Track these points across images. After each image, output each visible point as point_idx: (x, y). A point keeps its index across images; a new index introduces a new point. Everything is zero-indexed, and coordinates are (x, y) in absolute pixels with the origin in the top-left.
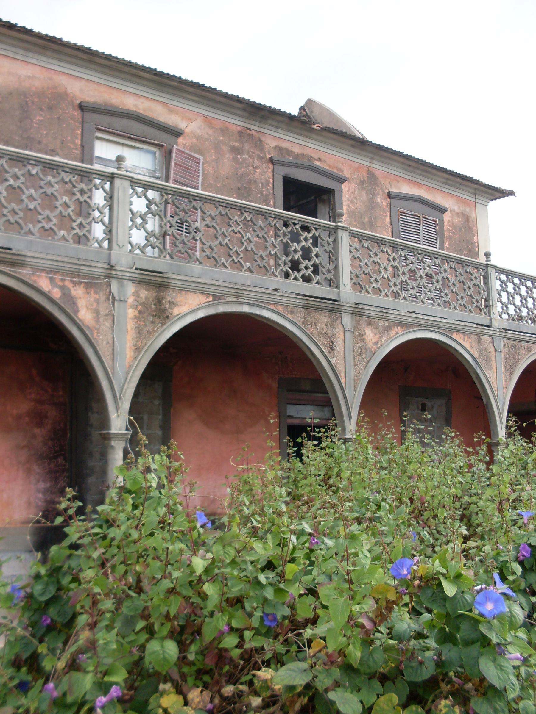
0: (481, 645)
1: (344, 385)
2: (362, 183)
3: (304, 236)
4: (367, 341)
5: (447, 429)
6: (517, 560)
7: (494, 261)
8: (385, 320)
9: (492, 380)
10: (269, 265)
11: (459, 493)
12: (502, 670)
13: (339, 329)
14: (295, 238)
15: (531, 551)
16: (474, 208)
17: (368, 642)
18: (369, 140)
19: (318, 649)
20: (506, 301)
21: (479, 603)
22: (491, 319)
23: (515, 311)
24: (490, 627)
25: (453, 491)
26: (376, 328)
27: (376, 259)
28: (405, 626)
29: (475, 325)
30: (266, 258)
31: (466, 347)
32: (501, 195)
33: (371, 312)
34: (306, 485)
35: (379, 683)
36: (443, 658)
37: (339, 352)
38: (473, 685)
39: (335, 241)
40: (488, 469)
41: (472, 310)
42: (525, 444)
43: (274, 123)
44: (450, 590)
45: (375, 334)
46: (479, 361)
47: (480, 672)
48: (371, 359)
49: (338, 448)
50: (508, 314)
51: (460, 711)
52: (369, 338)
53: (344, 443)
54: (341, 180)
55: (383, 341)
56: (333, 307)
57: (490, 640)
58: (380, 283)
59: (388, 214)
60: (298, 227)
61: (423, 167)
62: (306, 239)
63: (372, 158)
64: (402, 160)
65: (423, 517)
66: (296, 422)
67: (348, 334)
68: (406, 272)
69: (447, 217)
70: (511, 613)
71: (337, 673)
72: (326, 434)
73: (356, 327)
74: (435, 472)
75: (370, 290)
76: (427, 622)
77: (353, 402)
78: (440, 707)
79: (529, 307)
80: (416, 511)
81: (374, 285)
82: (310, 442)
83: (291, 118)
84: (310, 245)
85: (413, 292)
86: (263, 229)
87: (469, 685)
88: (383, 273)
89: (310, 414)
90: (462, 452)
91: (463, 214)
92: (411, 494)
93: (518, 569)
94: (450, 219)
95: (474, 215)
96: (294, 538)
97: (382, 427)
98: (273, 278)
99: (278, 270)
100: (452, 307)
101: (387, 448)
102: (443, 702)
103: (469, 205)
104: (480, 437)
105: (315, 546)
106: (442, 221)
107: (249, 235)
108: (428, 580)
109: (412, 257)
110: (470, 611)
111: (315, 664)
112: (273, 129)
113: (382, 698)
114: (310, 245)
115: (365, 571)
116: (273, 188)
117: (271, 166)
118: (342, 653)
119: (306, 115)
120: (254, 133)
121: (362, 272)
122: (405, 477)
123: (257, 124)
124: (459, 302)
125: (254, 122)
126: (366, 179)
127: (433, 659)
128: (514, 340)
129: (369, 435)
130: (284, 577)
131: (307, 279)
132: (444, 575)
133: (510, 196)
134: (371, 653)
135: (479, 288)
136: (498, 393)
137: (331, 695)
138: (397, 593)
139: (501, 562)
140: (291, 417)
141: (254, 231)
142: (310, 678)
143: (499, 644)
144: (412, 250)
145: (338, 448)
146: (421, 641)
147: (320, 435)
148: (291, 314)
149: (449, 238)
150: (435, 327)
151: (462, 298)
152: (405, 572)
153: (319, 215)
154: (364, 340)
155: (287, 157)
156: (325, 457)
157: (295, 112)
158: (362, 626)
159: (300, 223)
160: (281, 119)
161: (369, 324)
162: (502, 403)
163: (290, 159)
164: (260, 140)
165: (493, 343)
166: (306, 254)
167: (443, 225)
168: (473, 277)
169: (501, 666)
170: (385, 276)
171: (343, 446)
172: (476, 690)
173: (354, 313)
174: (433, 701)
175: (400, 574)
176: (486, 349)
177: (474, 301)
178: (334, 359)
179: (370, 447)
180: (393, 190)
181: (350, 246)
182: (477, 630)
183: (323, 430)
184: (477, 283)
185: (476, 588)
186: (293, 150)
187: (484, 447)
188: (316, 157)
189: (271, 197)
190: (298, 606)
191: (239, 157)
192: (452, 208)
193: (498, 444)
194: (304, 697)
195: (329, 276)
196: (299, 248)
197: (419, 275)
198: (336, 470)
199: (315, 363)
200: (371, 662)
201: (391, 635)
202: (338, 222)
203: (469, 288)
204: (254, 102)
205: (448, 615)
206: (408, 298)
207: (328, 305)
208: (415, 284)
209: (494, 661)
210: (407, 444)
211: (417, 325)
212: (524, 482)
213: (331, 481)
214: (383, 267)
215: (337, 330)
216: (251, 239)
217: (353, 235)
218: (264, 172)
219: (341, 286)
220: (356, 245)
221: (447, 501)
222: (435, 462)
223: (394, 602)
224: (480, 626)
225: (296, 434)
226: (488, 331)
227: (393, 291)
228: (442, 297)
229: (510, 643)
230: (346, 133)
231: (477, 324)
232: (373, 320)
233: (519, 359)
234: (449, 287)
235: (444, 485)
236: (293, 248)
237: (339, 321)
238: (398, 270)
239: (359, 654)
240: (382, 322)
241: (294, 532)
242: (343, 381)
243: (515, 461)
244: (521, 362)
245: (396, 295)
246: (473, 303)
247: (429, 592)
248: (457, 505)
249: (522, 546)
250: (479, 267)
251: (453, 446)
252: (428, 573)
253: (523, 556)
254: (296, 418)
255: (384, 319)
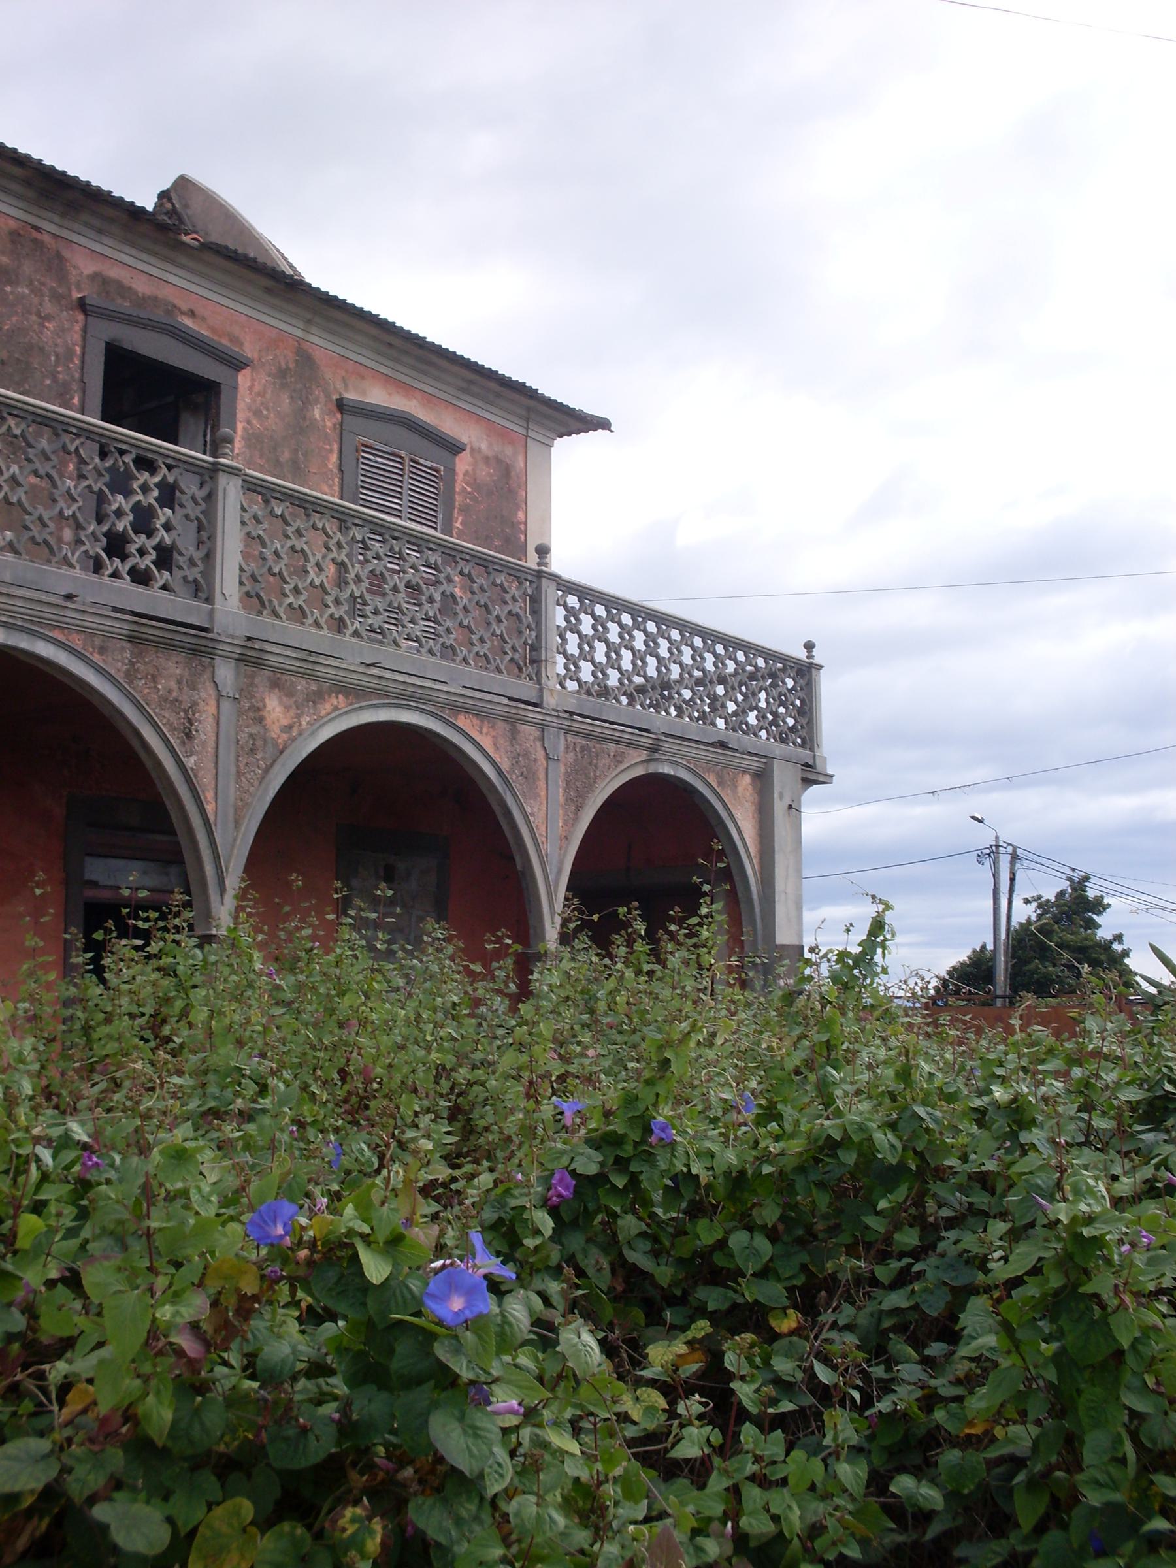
0: (436, 1387)
1: (212, 818)
2: (282, 373)
3: (141, 481)
4: (268, 721)
5: (430, 924)
6: (545, 1203)
7: (558, 564)
8: (310, 678)
9: (538, 821)
10: (60, 540)
11: (450, 1060)
12: (476, 1436)
13: (206, 693)
14: (121, 484)
15: (575, 1186)
16: (522, 450)
17: (192, 1386)
18: (308, 280)
19: (80, 1407)
20: (576, 652)
21: (432, 1296)
22: (541, 690)
23: (594, 674)
24: (458, 1349)
25: (434, 1056)
26: (290, 694)
27: (300, 544)
28: (286, 1350)
29: (506, 701)
30: (51, 525)
31: (483, 746)
32: (580, 426)
33: (281, 660)
34: (110, 1037)
35: (213, 1478)
36: (355, 1417)
37: (204, 744)
38: (415, 1472)
39: (210, 497)
40: (514, 1010)
41: (503, 668)
42: (595, 959)
43: (97, 223)
44: (375, 1269)
45: (287, 708)
46: (512, 778)
47: (430, 1445)
48: (275, 761)
49: (187, 956)
50: (579, 681)
51: (384, 1528)
52: (274, 716)
53: (200, 946)
54: (237, 364)
55: (304, 723)
56: (198, 644)
57: (458, 1376)
58: (303, 597)
59: (336, 447)
60: (128, 459)
61: (419, 352)
62: (145, 488)
63: (309, 322)
64: (374, 331)
65: (368, 1112)
66: (105, 895)
67: (226, 705)
68: (363, 575)
69: (463, 464)
70: (504, 1316)
71: (116, 1458)
72: (161, 924)
73: (246, 691)
74: (396, 1014)
75: (280, 611)
76: (331, 1339)
77: (230, 856)
78: (342, 1522)
79: (624, 668)
80: (354, 1099)
81: (291, 599)
82: (124, 942)
83: (134, 212)
84: (153, 501)
85: (375, 621)
86: (48, 459)
87: (409, 1472)
88: (312, 574)
89: (131, 879)
90: (459, 973)
91: (498, 460)
92: (343, 1061)
93: (546, 1223)
94: (470, 469)
95: (522, 464)
96: (46, 1155)
97: (288, 914)
98: (65, 570)
99: (77, 554)
100: (458, 659)
101: (299, 959)
102: (349, 1512)
103: (512, 442)
104: (499, 940)
105: (94, 1172)
106: (451, 471)
107: (15, 469)
108: (331, 1249)
109: (378, 545)
110: (418, 1314)
111: (69, 1441)
112: (92, 234)
113: (218, 1511)
114: (153, 501)
115: (187, 1230)
116: (82, 369)
117: (81, 317)
118: (129, 1415)
119: (174, 212)
120: (46, 238)
121: (265, 569)
122: (332, 1025)
123: (57, 218)
124: (476, 649)
125: (49, 215)
126: (292, 365)
127: (333, 1420)
128: (588, 736)
129: (257, 930)
130: (13, 1244)
131: (141, 578)
132: (364, 1237)
133: (600, 431)
134: (197, 1412)
135: (520, 621)
136: (549, 848)
137: (100, 1512)
138: (262, 1277)
139: (513, 1209)
140: (94, 884)
141: (29, 460)
142: (54, 1473)
143: (472, 1383)
144: (379, 528)
145: (187, 956)
146: (321, 1381)
147: (146, 926)
148: (101, 653)
149: (465, 510)
150: (419, 699)
151: (448, 631)
152: (280, 1231)
153: (181, 438)
154: (260, 720)
155: (119, 301)
156: (155, 976)
157: (147, 201)
158: (179, 1352)
159: (134, 451)
160: (110, 212)
161: (275, 684)
162: (555, 870)
163: (124, 305)
164: (59, 256)
165: (542, 740)
166: (143, 521)
167: (454, 481)
168: (508, 597)
169: (475, 1428)
170: (317, 583)
171: (198, 951)
172: (421, 1481)
173: (242, 659)
174: (330, 1511)
175: (268, 1237)
176: (526, 754)
177: (508, 647)
178: (193, 759)
179: (257, 955)
180: (351, 395)
181: (243, 509)
182: (429, 1353)
183: (154, 915)
184: (516, 609)
185: (432, 1265)
186: (134, 286)
187: (509, 962)
188: (184, 308)
189: (75, 387)
190: (43, 1310)
191: (8, 289)
192: (476, 445)
193: (541, 957)
194: (41, 1518)
195: (193, 573)
196: (127, 507)
197: (392, 584)
198: (179, 1004)
199: (149, 764)
200: (196, 1432)
201: (251, 1368)
202: (224, 455)
203: (499, 619)
204: (52, 168)
205: (370, 1324)
206: (365, 634)
207: (186, 637)
208: (379, 603)
209: (461, 1419)
210: (338, 950)
211: (380, 693)
212: (586, 1038)
213: (166, 1030)
214: (313, 560)
215: (203, 695)
216: (20, 479)
217: (252, 487)
218: (63, 330)
219: (218, 597)
220: (257, 508)
221: (422, 1078)
222: (400, 994)
223: (255, 1298)
224: (436, 1345)
225: (100, 922)
226: (533, 714)
227: (331, 616)
228: (439, 636)
229: (496, 1380)
230: (255, 260)
231: (510, 699)
232: (285, 677)
233: (596, 777)
234: (456, 614)
235: (417, 1043)
236: (114, 507)
237: (207, 675)
238: (347, 571)
239: (168, 1415)
240: (303, 682)
241: (49, 1142)
242: (210, 808)
243: (572, 995)
244: (601, 784)
245: (339, 625)
246: (506, 653)
247: (332, 1275)
248: (445, 1085)
249: (557, 1176)
250: (523, 576)
251: (439, 960)
252: (330, 1232)
253: (560, 1195)
254: (105, 887)
255: (309, 676)
